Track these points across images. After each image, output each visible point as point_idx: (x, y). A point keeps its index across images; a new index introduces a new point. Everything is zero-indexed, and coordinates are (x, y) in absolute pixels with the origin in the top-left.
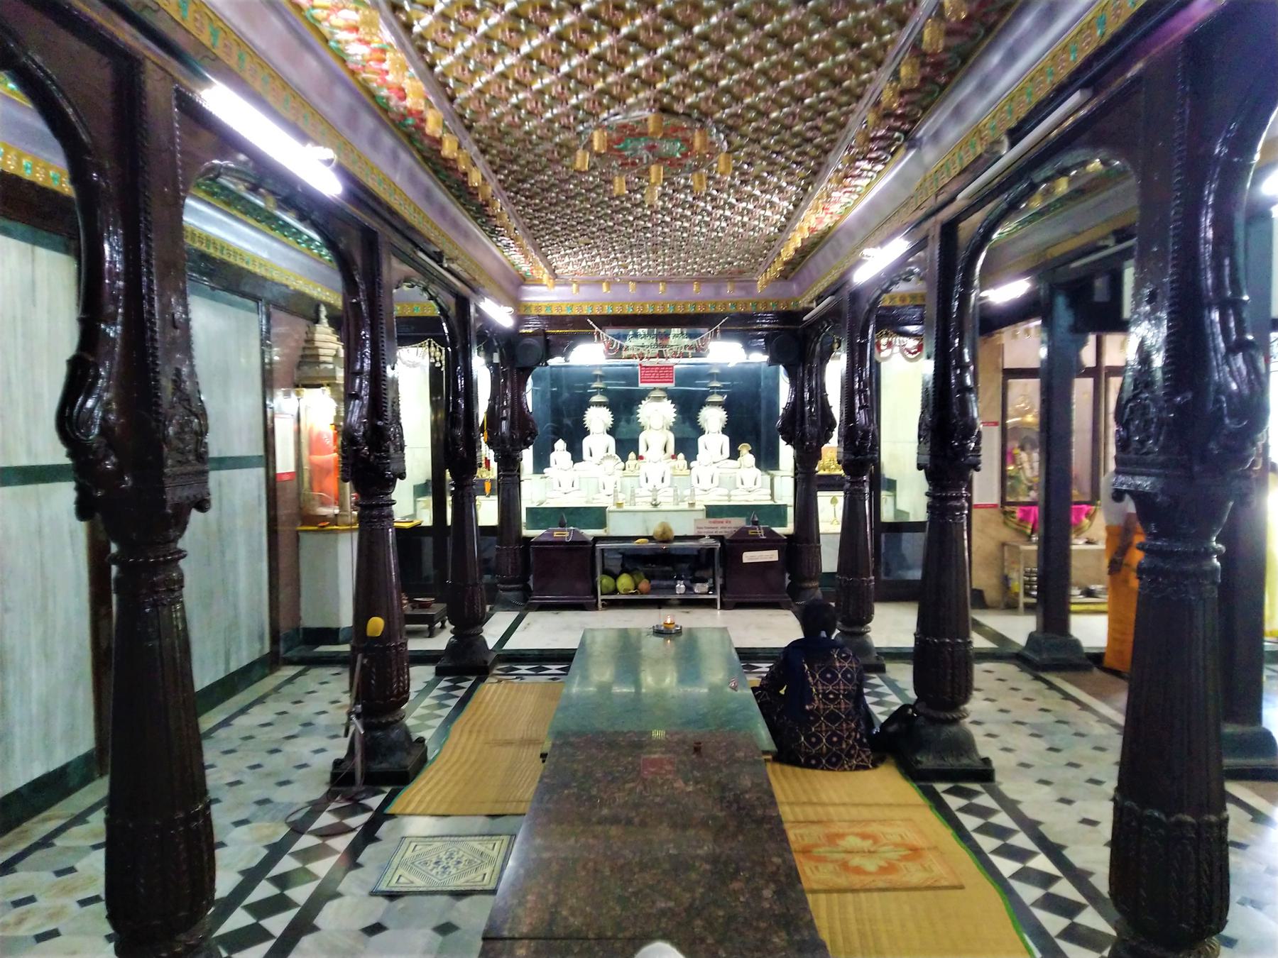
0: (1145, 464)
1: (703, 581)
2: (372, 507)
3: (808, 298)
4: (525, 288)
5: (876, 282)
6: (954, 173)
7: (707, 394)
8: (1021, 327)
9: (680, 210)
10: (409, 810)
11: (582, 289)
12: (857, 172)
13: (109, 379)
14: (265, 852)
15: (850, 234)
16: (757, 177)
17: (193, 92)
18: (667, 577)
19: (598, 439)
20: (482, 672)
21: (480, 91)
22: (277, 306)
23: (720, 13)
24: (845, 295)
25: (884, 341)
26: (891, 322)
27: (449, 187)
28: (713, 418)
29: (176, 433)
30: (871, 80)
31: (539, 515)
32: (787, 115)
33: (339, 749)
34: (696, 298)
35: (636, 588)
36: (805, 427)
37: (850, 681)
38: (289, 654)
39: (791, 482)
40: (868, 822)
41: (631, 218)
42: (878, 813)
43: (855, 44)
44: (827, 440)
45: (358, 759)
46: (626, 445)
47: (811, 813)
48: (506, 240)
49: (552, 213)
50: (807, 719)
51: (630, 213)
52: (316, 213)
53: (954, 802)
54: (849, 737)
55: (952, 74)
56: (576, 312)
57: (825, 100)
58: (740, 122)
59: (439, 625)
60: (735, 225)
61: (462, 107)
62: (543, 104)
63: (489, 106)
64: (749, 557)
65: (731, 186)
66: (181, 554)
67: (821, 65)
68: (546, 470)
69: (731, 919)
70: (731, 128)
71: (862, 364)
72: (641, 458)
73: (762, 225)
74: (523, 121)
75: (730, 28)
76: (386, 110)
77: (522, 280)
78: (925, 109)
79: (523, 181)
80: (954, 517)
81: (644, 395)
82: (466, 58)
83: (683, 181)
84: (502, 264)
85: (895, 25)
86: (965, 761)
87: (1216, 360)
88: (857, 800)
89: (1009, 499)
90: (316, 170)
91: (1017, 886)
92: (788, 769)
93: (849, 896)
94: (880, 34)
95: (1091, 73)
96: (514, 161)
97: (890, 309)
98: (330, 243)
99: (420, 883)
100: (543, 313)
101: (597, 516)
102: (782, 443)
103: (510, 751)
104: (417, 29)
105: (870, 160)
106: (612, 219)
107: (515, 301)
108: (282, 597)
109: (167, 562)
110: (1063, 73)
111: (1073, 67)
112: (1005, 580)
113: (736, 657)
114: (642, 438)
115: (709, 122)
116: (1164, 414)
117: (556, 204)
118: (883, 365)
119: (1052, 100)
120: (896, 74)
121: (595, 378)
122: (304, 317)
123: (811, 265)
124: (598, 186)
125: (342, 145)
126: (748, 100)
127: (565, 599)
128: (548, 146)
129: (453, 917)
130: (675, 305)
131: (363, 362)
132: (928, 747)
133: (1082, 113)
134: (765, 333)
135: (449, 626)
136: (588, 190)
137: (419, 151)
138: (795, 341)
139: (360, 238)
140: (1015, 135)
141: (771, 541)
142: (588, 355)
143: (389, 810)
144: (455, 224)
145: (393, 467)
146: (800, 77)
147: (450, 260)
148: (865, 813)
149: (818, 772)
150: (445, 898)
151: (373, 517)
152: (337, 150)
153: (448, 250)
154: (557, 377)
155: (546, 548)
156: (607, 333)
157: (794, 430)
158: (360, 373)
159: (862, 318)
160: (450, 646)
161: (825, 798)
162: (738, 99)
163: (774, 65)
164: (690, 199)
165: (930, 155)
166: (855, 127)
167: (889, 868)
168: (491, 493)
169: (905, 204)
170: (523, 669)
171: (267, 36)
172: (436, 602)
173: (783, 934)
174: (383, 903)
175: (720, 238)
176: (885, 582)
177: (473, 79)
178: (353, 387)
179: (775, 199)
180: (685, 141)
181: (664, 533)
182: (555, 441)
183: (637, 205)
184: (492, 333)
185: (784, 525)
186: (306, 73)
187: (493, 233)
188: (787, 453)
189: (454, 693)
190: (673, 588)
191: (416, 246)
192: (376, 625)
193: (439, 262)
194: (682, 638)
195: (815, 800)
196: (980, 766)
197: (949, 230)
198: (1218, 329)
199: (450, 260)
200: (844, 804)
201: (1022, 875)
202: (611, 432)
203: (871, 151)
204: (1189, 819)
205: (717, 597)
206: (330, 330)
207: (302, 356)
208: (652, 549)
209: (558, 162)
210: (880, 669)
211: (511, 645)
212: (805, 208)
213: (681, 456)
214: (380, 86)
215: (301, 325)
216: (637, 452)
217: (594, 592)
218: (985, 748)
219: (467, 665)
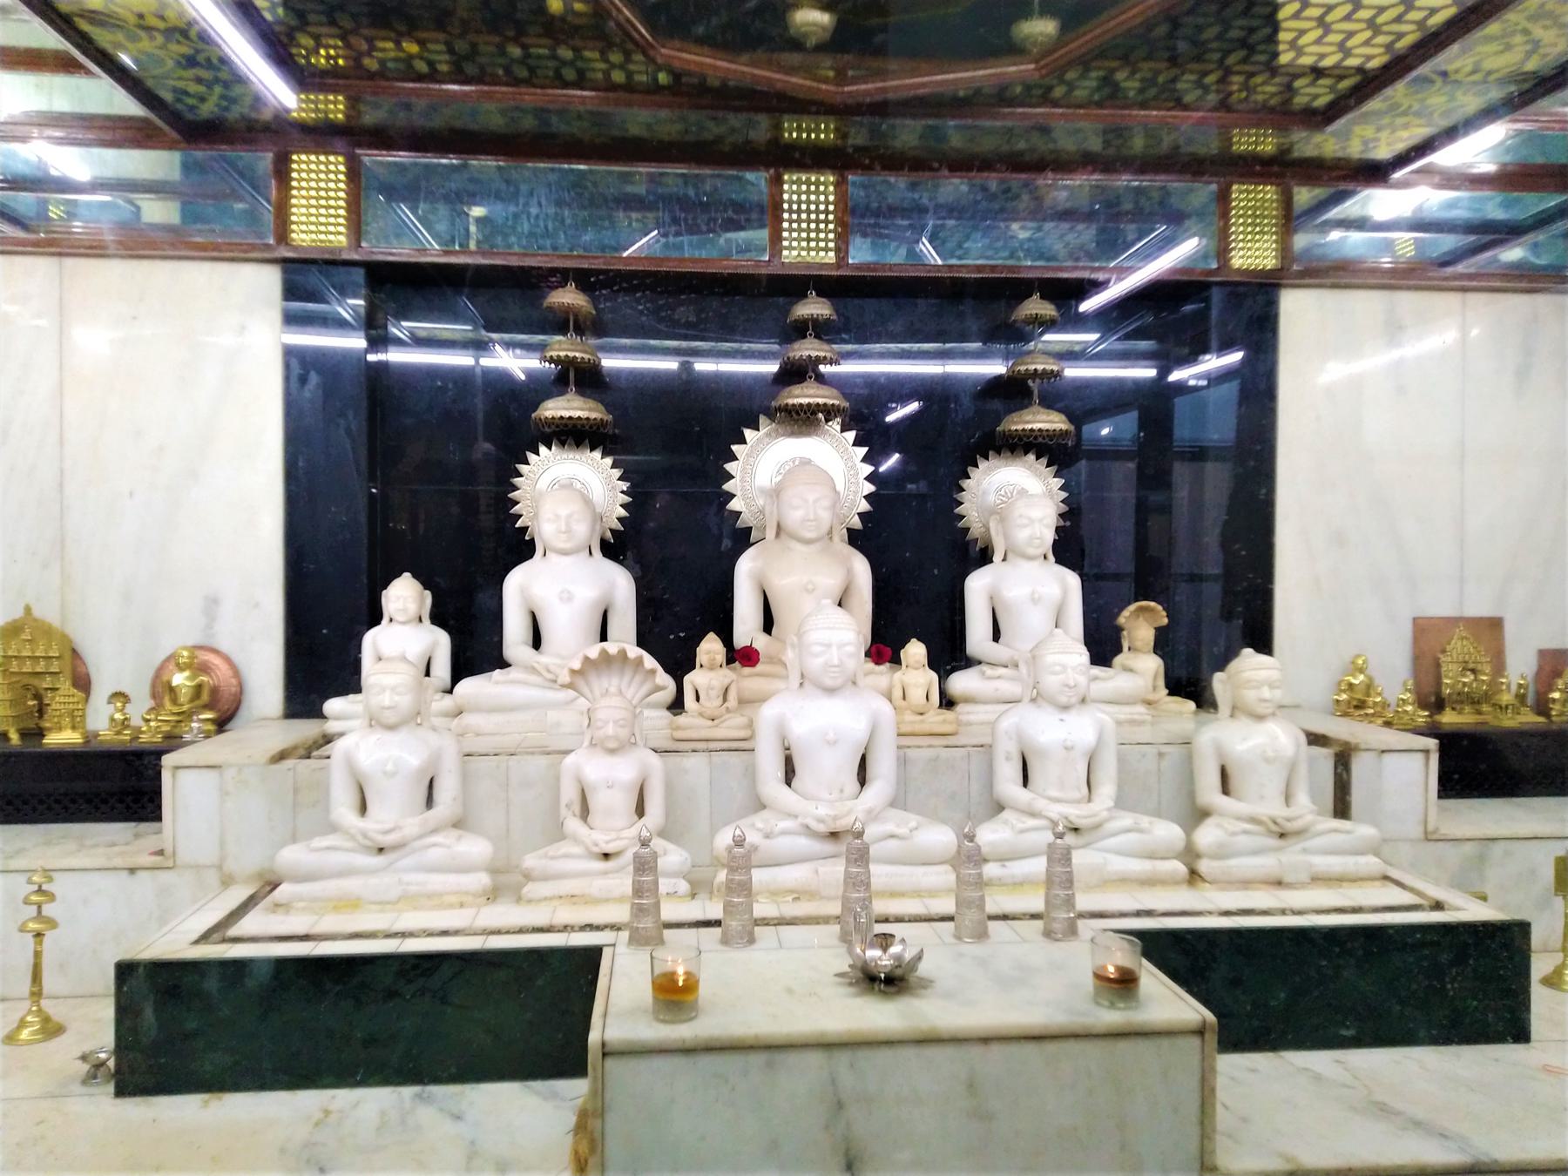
19: (566, 584)
28: (1015, 499)
46: (683, 587)
68: (333, 705)
72: (748, 657)
216: (727, 637)
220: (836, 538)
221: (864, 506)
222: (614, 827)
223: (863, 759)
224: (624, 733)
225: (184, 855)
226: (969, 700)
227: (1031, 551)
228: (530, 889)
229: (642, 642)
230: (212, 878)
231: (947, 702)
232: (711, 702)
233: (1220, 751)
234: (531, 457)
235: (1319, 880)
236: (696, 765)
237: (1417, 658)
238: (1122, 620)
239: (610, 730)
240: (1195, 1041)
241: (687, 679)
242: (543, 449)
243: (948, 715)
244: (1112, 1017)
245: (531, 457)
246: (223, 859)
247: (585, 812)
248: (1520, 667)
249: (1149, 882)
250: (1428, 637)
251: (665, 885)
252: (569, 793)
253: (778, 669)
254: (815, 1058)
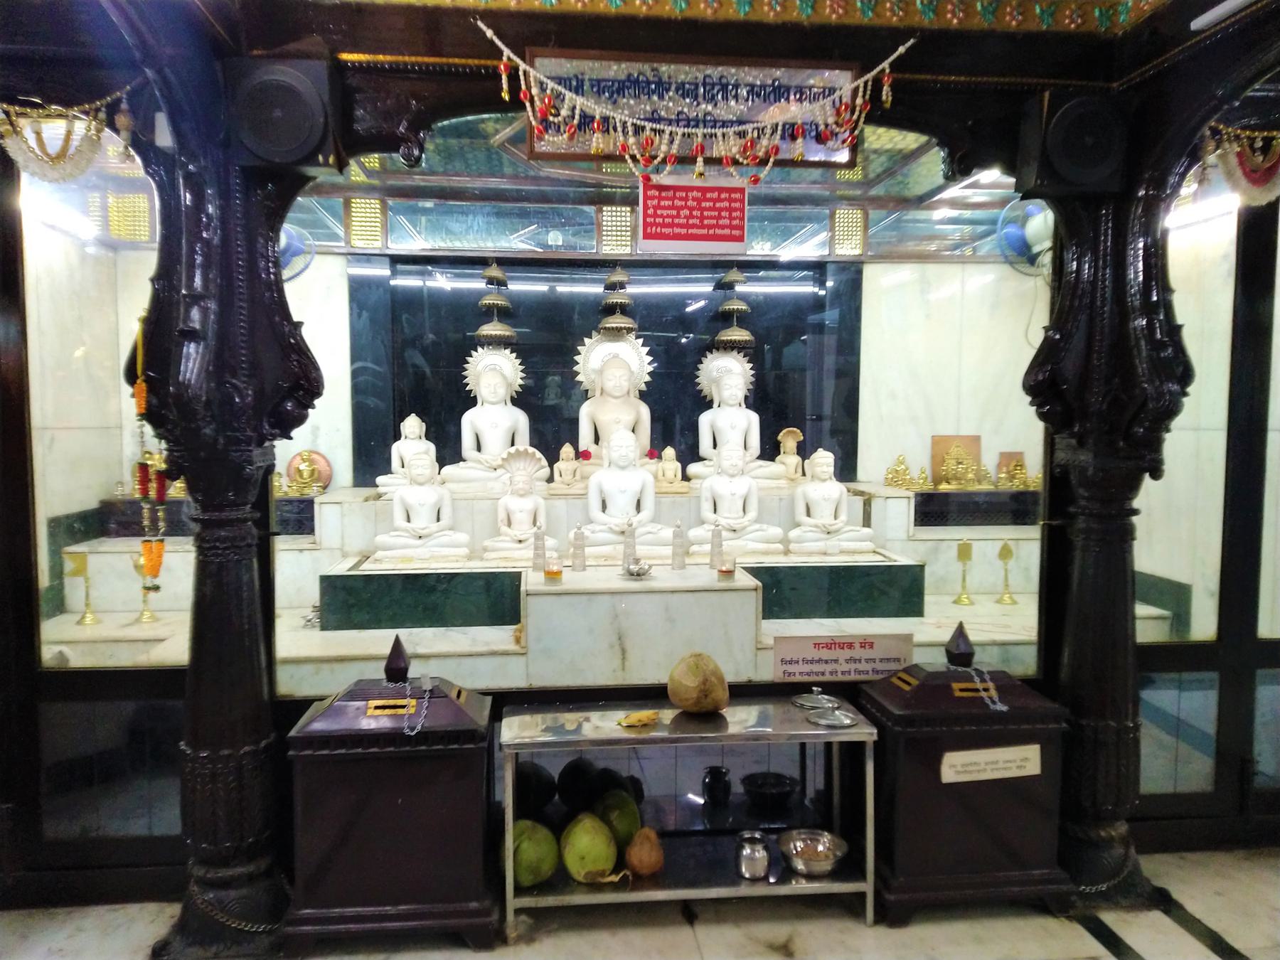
19: (493, 419)
28: (727, 375)
35: (621, 862)
46: (552, 420)
64: (958, 766)
68: (380, 480)
72: (586, 455)
114: (586, 413)
216: (575, 444)
220: (632, 395)
221: (648, 378)
222: (523, 528)
223: (639, 501)
224: (527, 487)
225: (325, 544)
226: (697, 477)
227: (731, 402)
228: (486, 555)
229: (532, 445)
230: (338, 553)
231: (686, 478)
232: (568, 477)
233: (805, 497)
234: (474, 353)
235: (842, 552)
236: (560, 504)
237: (933, 457)
238: (779, 438)
239: (521, 485)
240: (754, 593)
241: (555, 466)
242: (480, 349)
243: (686, 483)
244: (724, 585)
245: (474, 353)
246: (343, 545)
247: (509, 524)
248: (989, 461)
249: (766, 553)
250: (940, 445)
251: (548, 554)
252: (502, 515)
253: (598, 461)
254: (606, 597)
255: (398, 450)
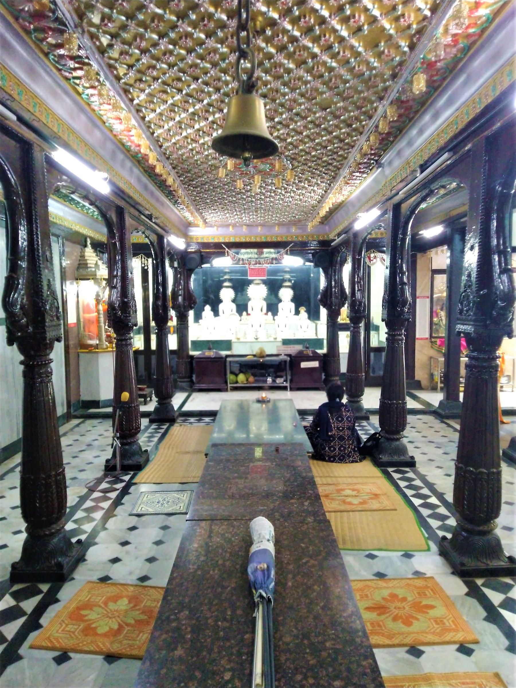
0: (468, 321)
1: (281, 377)
2: (122, 340)
3: (333, 234)
4: (191, 228)
5: (366, 229)
6: (398, 181)
7: (284, 280)
8: (440, 249)
9: (269, 193)
10: (143, 481)
11: (219, 229)
12: (354, 178)
13: (23, 285)
14: (78, 499)
15: (352, 204)
16: (306, 179)
17: (50, 154)
18: (263, 375)
20: (172, 421)
21: (175, 144)
22: (67, 240)
23: (287, 114)
24: (351, 235)
25: (372, 255)
26: (374, 245)
27: (156, 183)
28: (286, 294)
29: (50, 308)
30: (358, 140)
31: (197, 344)
32: (319, 154)
33: (108, 454)
34: (277, 233)
35: (247, 380)
36: (331, 299)
37: (350, 421)
38: (75, 413)
39: (325, 327)
40: (356, 484)
41: (245, 197)
42: (360, 480)
43: (350, 126)
44: (343, 306)
45: (118, 458)
46: (242, 307)
47: (329, 480)
48: (182, 207)
49: (206, 194)
50: (329, 439)
51: (244, 195)
52: (98, 202)
53: (396, 476)
54: (349, 447)
55: (396, 137)
56: (216, 240)
57: (337, 147)
58: (297, 156)
59: (149, 399)
60: (296, 200)
61: (166, 150)
62: (204, 149)
63: (178, 149)
64: (304, 365)
65: (293, 183)
66: (51, 361)
67: (334, 134)
68: (200, 321)
69: (290, 513)
70: (293, 159)
71: (359, 268)
72: (249, 314)
73: (309, 200)
74: (194, 156)
75: (291, 119)
76: (129, 151)
77: (189, 225)
78: (385, 151)
79: (192, 181)
80: (398, 344)
81: (250, 282)
82: (169, 130)
83: (270, 181)
84: (179, 217)
85: (367, 118)
86: (402, 458)
87: (496, 275)
88: (351, 475)
89: (434, 335)
90: (100, 183)
91: (421, 509)
92: (320, 463)
93: (345, 514)
94: (361, 121)
95: (454, 145)
96: (189, 172)
97: (375, 239)
98: (103, 215)
99: (151, 510)
100: (199, 241)
101: (227, 344)
102: (321, 307)
103: (188, 457)
104: (147, 119)
105: (360, 172)
106: (235, 197)
107: (185, 235)
108: (72, 385)
109: (46, 364)
110: (442, 142)
111: (446, 140)
112: (432, 376)
113: (297, 414)
115: (283, 156)
116: (475, 299)
117: (208, 191)
118: (372, 268)
119: (438, 154)
120: (368, 140)
121: (226, 273)
122: (81, 245)
123: (335, 217)
124: (229, 183)
125: (109, 169)
126: (301, 148)
127: (212, 386)
128: (206, 166)
129: (168, 523)
130: (266, 237)
131: (117, 270)
132: (385, 452)
133: (449, 162)
134: (312, 251)
135: (154, 398)
136: (224, 185)
137: (142, 167)
138: (327, 255)
139: (116, 213)
140: (423, 168)
141: (315, 357)
142: (222, 263)
143: (134, 481)
144: (158, 200)
145: (133, 321)
146: (324, 138)
147: (156, 218)
148: (355, 480)
149: (334, 464)
150: (164, 516)
151: (123, 345)
152: (107, 171)
153: (155, 214)
154: (205, 273)
155: (201, 360)
156: (232, 252)
157: (327, 300)
158: (116, 276)
159: (359, 247)
160: (156, 409)
161: (336, 475)
162: (296, 147)
163: (313, 134)
164: (274, 188)
165: (388, 171)
166: (351, 160)
167: (364, 503)
168: (174, 333)
169: (378, 193)
170: (192, 420)
171: (80, 124)
172: (148, 387)
173: (312, 518)
174: (136, 518)
175: (289, 206)
176: (372, 377)
177: (171, 138)
178: (113, 283)
179: (315, 188)
180: (271, 164)
181: (261, 353)
182: (204, 306)
183: (248, 191)
184: (174, 252)
185: (322, 348)
186: (95, 137)
187: (176, 203)
188: (323, 312)
189: (159, 431)
190: (266, 381)
191: (140, 212)
192: (125, 396)
193: (151, 219)
194: (270, 405)
195: (332, 475)
196: (409, 460)
197: (397, 208)
198: (496, 263)
199: (156, 218)
200: (345, 477)
201: (423, 505)
202: (234, 301)
203: (360, 168)
204: (485, 471)
205: (288, 385)
206: (92, 251)
207: (79, 264)
208: (255, 361)
209: (210, 173)
210: (367, 418)
211: (186, 408)
212: (330, 193)
213: (270, 313)
214: (128, 141)
215: (78, 248)
216: (247, 311)
217: (226, 382)
218: (411, 451)
219: (165, 417)
255: (204, 314)
